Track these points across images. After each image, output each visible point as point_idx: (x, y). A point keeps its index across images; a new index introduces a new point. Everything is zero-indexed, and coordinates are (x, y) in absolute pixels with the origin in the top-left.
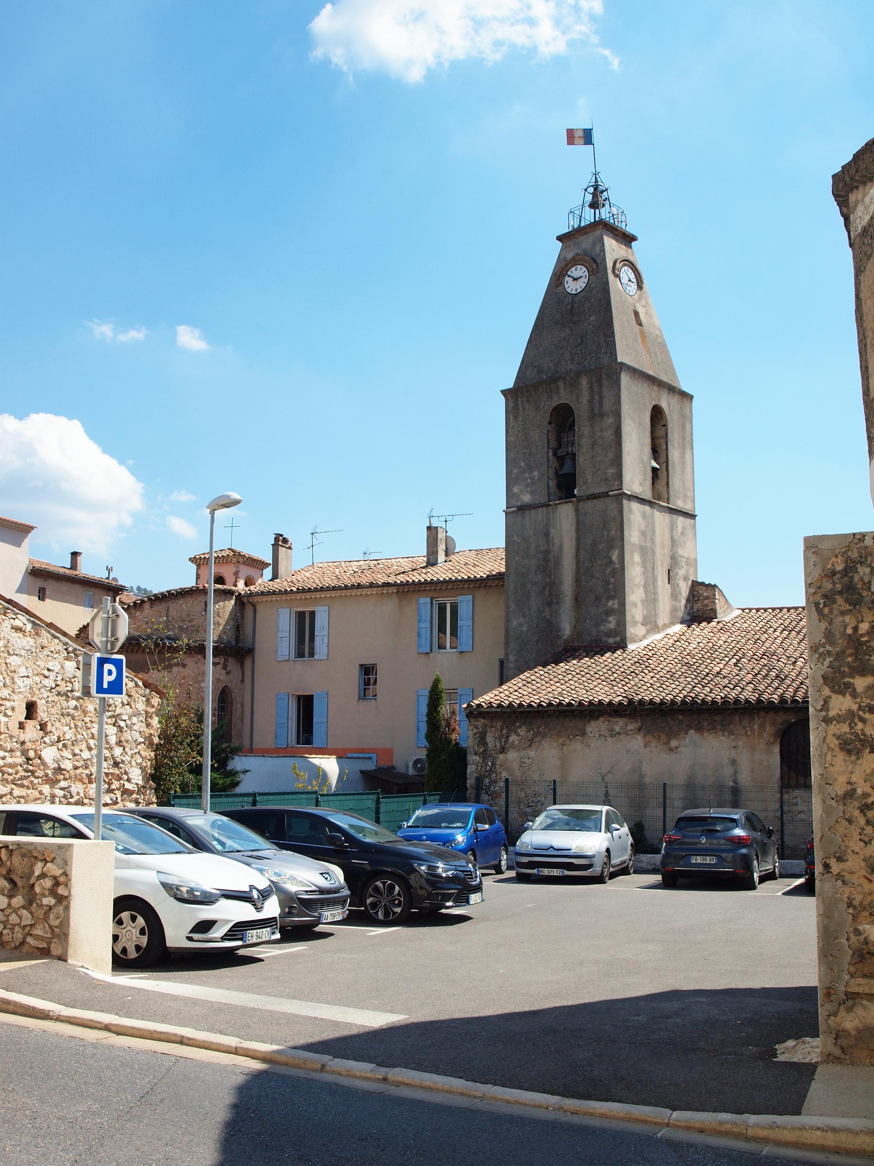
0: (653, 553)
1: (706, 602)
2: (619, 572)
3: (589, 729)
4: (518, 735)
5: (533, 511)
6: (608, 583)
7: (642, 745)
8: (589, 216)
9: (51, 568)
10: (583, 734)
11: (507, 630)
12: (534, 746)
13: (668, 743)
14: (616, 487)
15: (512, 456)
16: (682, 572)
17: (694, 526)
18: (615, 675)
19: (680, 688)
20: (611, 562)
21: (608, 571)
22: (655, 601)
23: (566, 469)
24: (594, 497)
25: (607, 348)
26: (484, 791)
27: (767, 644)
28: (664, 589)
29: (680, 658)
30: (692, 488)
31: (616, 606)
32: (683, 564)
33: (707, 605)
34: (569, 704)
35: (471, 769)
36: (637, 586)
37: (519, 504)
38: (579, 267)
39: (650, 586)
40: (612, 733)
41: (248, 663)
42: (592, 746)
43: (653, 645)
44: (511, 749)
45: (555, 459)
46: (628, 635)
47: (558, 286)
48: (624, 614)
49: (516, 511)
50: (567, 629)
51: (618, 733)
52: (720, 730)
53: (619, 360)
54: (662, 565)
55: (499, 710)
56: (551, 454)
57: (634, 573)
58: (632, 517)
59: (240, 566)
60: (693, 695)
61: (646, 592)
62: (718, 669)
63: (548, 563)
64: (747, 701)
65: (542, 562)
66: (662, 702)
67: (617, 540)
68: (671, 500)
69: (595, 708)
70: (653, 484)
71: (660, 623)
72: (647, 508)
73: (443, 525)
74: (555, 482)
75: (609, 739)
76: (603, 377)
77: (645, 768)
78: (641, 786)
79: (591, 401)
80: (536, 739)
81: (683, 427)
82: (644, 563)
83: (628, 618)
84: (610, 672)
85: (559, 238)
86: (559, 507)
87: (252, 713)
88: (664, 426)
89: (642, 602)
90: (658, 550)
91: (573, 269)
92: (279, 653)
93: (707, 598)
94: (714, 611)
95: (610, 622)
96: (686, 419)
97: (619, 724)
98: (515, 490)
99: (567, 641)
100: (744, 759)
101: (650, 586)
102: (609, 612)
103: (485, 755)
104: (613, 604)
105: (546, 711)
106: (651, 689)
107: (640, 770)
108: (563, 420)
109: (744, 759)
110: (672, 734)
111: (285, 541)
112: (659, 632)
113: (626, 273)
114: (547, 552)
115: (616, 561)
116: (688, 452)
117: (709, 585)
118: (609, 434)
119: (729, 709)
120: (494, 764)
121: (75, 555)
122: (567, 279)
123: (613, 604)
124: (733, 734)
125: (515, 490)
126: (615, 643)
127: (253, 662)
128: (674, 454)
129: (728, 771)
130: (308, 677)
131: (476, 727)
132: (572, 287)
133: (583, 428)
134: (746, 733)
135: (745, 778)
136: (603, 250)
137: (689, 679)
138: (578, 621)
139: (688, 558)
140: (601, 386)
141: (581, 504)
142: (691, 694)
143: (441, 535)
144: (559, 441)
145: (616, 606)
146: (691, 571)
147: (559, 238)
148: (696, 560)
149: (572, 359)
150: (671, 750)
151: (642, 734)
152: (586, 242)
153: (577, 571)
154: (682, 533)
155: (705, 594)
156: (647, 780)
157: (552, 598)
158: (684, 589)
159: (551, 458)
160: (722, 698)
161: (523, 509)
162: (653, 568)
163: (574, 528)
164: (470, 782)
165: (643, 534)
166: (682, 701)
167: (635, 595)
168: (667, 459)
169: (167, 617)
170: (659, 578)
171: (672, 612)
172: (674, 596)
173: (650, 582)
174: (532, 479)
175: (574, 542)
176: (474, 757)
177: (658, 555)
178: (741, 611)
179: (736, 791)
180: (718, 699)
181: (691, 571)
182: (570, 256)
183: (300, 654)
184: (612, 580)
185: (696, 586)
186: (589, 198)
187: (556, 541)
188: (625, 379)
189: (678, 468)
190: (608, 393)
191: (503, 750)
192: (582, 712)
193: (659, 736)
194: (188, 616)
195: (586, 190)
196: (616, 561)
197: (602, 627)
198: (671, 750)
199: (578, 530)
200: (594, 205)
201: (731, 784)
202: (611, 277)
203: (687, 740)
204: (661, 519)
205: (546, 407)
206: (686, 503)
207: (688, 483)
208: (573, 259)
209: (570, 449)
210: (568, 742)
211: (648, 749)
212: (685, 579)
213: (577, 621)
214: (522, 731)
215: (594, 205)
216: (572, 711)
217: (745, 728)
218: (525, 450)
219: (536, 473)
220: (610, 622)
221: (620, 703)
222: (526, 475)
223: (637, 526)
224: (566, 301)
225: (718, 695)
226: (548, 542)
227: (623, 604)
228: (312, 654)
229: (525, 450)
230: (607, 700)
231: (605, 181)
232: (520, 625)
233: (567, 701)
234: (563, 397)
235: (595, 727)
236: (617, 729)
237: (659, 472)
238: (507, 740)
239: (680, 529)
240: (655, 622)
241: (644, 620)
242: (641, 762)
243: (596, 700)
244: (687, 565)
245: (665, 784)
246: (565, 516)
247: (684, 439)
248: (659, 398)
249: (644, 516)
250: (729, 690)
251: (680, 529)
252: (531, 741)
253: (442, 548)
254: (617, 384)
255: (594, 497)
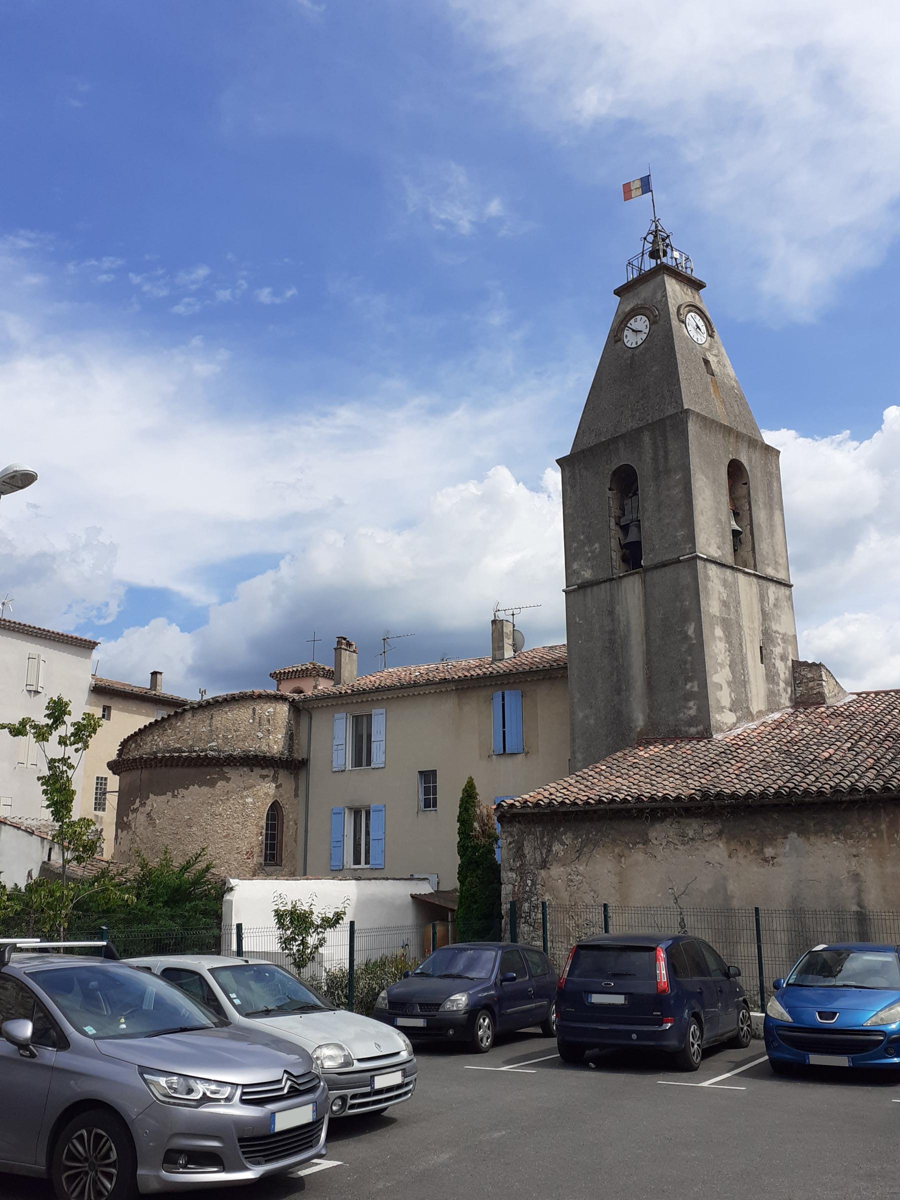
0: (740, 626)
1: (811, 684)
2: (697, 649)
3: (652, 834)
4: (563, 844)
5: (595, 588)
6: (686, 662)
7: (726, 855)
8: (649, 264)
9: (135, 689)
10: (646, 842)
11: (572, 725)
12: (583, 858)
13: (761, 851)
14: (688, 551)
15: (570, 530)
16: (778, 650)
17: (790, 598)
18: (693, 767)
19: (774, 778)
20: (686, 637)
21: (684, 648)
22: (744, 683)
23: (632, 537)
24: (664, 565)
25: (671, 398)
26: (523, 920)
27: (892, 725)
28: (756, 671)
29: (778, 746)
30: (784, 554)
31: (696, 689)
32: (779, 641)
33: (812, 688)
34: (624, 800)
35: (506, 889)
36: (722, 665)
37: (579, 581)
38: (639, 317)
39: (737, 664)
40: (684, 839)
41: (302, 775)
42: (659, 858)
43: (746, 734)
44: (555, 863)
45: (618, 529)
46: (713, 722)
47: (616, 342)
48: (706, 697)
49: (576, 590)
50: (640, 720)
51: (692, 839)
52: (833, 832)
53: (686, 407)
54: (752, 642)
55: (536, 810)
56: (613, 523)
57: (717, 649)
58: (710, 584)
59: (320, 679)
60: (791, 785)
61: (733, 672)
62: (826, 755)
63: (615, 645)
64: (868, 790)
65: (607, 645)
66: (748, 795)
67: (691, 611)
68: (758, 568)
69: (658, 805)
70: (735, 550)
71: (754, 709)
72: (728, 572)
73: (510, 618)
74: (619, 554)
75: (681, 847)
76: (668, 429)
77: (732, 886)
78: (727, 912)
79: (655, 459)
80: (585, 849)
81: (770, 485)
82: (728, 638)
83: (712, 702)
84: (687, 765)
85: (618, 292)
86: (625, 580)
87: (306, 831)
88: (746, 484)
89: (729, 683)
90: (745, 623)
91: (632, 321)
92: (334, 764)
93: (812, 680)
94: (821, 695)
95: (690, 708)
96: (773, 476)
97: (692, 827)
98: (575, 566)
99: (640, 733)
100: (870, 871)
101: (737, 664)
102: (689, 696)
103: (522, 872)
104: (692, 687)
105: (595, 811)
106: (736, 781)
107: (726, 890)
108: (626, 482)
109: (870, 871)
110: (765, 840)
111: (349, 644)
112: (753, 720)
113: (693, 319)
114: (613, 632)
115: (693, 636)
116: (777, 513)
117: (814, 664)
118: (677, 492)
119: (842, 802)
120: (534, 883)
121: (155, 674)
122: (626, 333)
123: (692, 687)
124: (852, 838)
125: (575, 566)
126: (698, 733)
127: (308, 774)
128: (760, 515)
129: (848, 890)
130: (364, 787)
131: (511, 835)
132: (631, 340)
133: (646, 487)
134: (870, 836)
135: (873, 899)
136: (665, 296)
137: (787, 768)
138: (652, 708)
139: (784, 635)
140: (666, 439)
141: (649, 575)
142: (788, 784)
143: (508, 629)
144: (622, 509)
145: (696, 689)
146: (790, 649)
147: (618, 292)
148: (795, 636)
149: (633, 416)
150: (766, 860)
151: (724, 840)
152: (645, 292)
153: (648, 652)
154: (775, 605)
155: (810, 675)
156: (736, 903)
157: (619, 686)
158: (783, 670)
159: (614, 528)
160: (831, 787)
161: (584, 586)
162: (741, 644)
163: (641, 603)
164: (505, 907)
165: (725, 604)
166: (775, 793)
167: (719, 677)
168: (751, 520)
169: (210, 726)
170: (749, 655)
171: (768, 696)
172: (771, 677)
173: (738, 660)
174: (593, 552)
175: (642, 620)
176: (510, 874)
177: (746, 630)
178: (855, 697)
179: (862, 918)
180: (827, 788)
181: (790, 649)
182: (628, 309)
183: (358, 762)
184: (689, 658)
185: (798, 666)
186: (648, 246)
187: (622, 618)
188: (693, 427)
189: (765, 532)
190: (672, 445)
191: (544, 865)
192: (641, 811)
193: (748, 842)
194: (233, 724)
195: (645, 239)
196: (693, 636)
197: (682, 715)
198: (766, 860)
199: (646, 604)
200: (654, 254)
201: (855, 908)
202: (675, 322)
203: (787, 847)
204: (746, 586)
205: (606, 472)
206: (778, 571)
207: (779, 548)
208: (633, 310)
209: (635, 516)
210: (626, 852)
211: (734, 860)
212: (783, 658)
213: (651, 708)
214: (568, 838)
215: (654, 254)
216: (629, 811)
217: (867, 828)
218: (584, 522)
219: (597, 545)
220: (690, 708)
221: (691, 798)
222: (586, 549)
223: (716, 595)
224: (626, 356)
225: (827, 784)
226: (613, 620)
227: (704, 685)
228: (369, 763)
229: (584, 522)
230: (674, 795)
231: (667, 225)
232: (586, 717)
233: (622, 796)
234: (623, 458)
235: (659, 832)
236: (691, 834)
237: (742, 536)
238: (549, 851)
239: (772, 600)
240: (748, 708)
241: (732, 705)
242: (725, 878)
243: (660, 795)
244: (784, 642)
245: (757, 909)
246: (632, 590)
247: (771, 499)
248: (737, 451)
249: (725, 583)
250: (841, 778)
251: (772, 600)
252: (580, 851)
253: (508, 642)
254: (684, 433)
255: (664, 565)
